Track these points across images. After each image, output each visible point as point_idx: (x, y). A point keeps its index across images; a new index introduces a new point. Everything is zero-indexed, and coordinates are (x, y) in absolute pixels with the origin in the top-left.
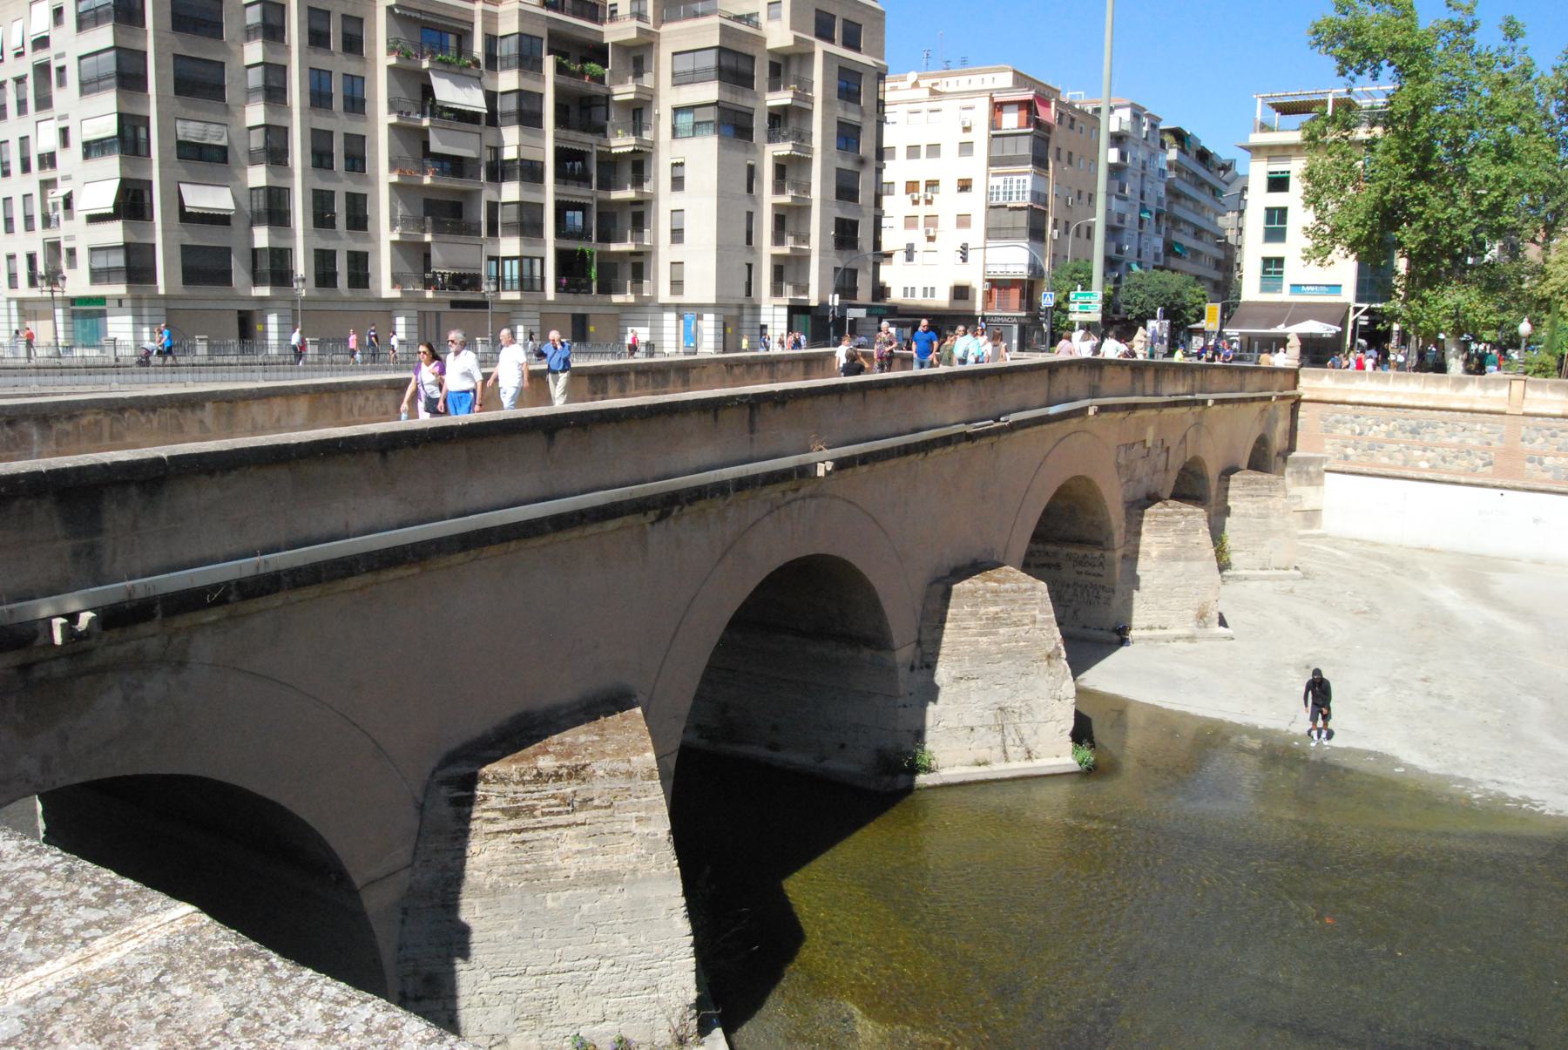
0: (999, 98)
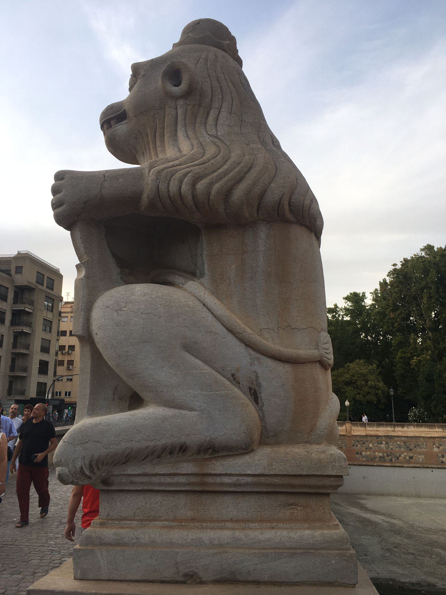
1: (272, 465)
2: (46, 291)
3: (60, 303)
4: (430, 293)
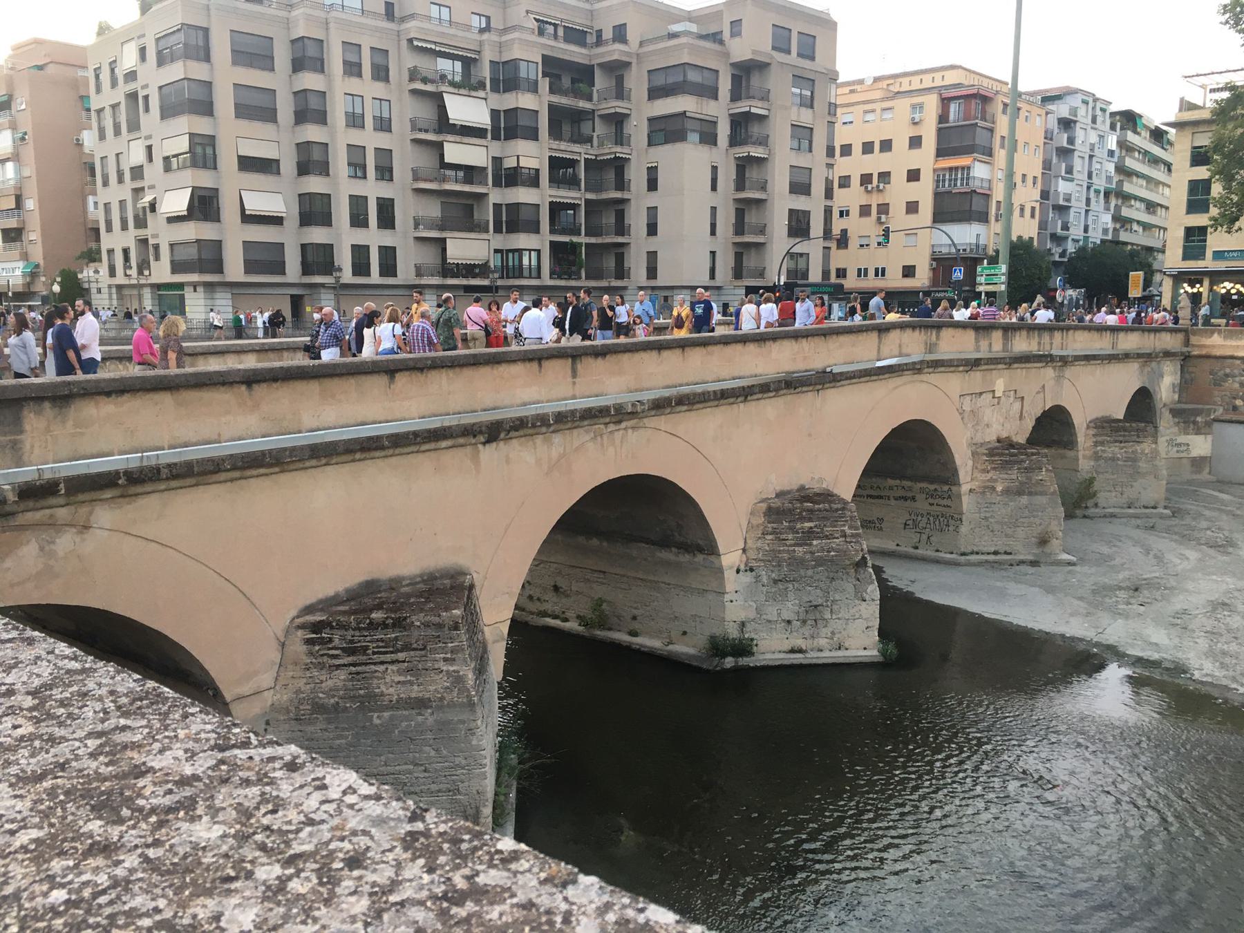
0: (946, 94)
2: (251, 53)
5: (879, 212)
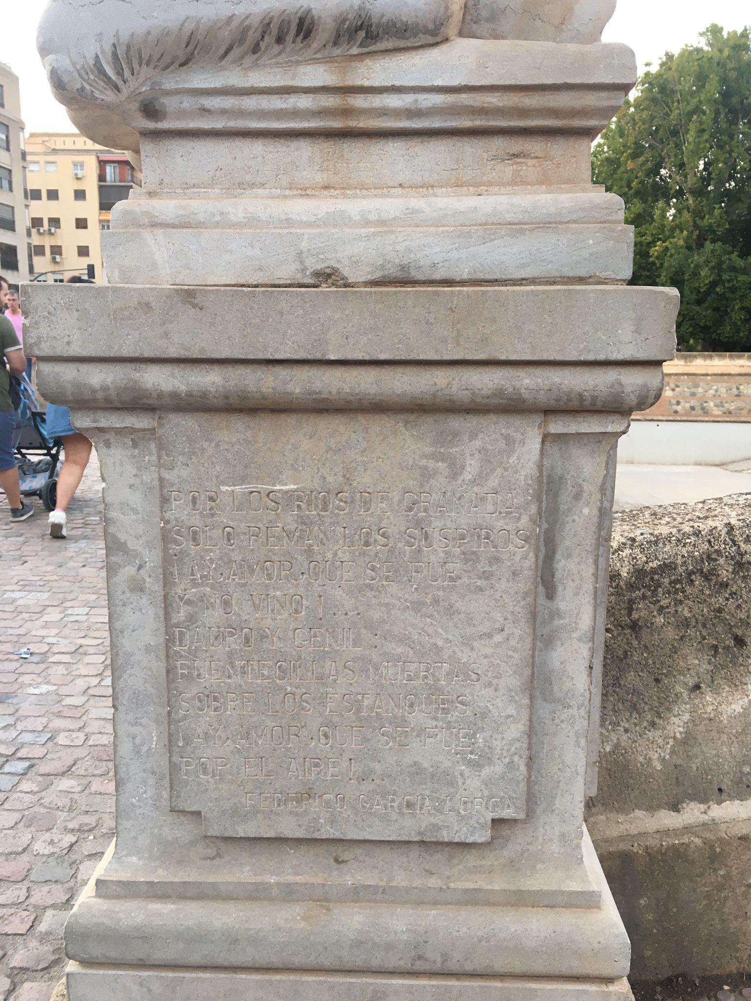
1: (487, 66)
3: (21, 134)
4: (701, 123)
5: (52, 253)
